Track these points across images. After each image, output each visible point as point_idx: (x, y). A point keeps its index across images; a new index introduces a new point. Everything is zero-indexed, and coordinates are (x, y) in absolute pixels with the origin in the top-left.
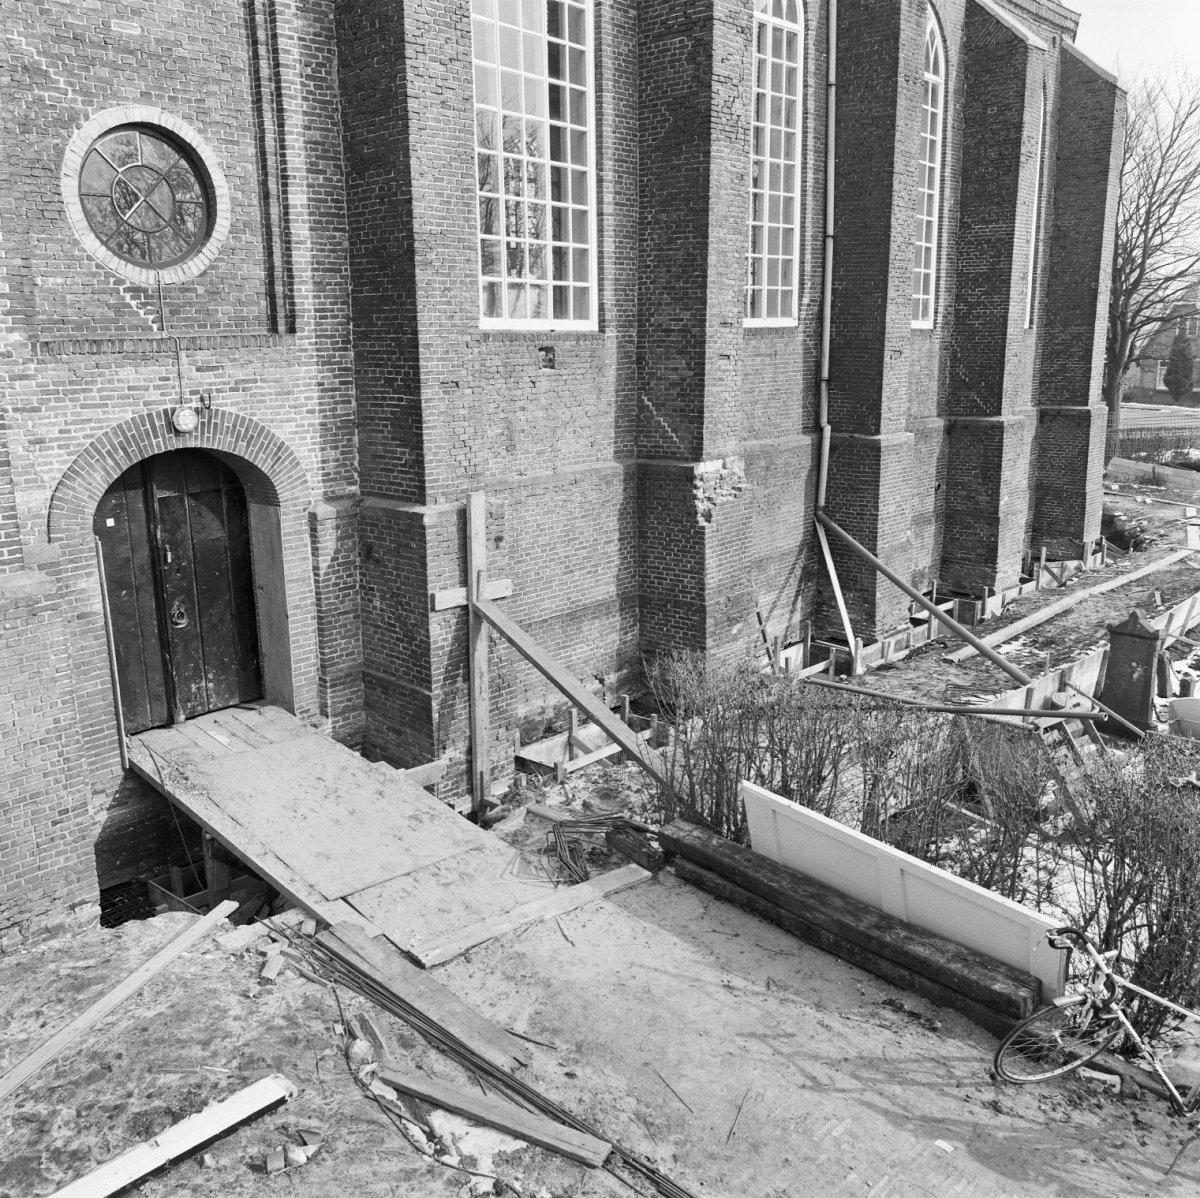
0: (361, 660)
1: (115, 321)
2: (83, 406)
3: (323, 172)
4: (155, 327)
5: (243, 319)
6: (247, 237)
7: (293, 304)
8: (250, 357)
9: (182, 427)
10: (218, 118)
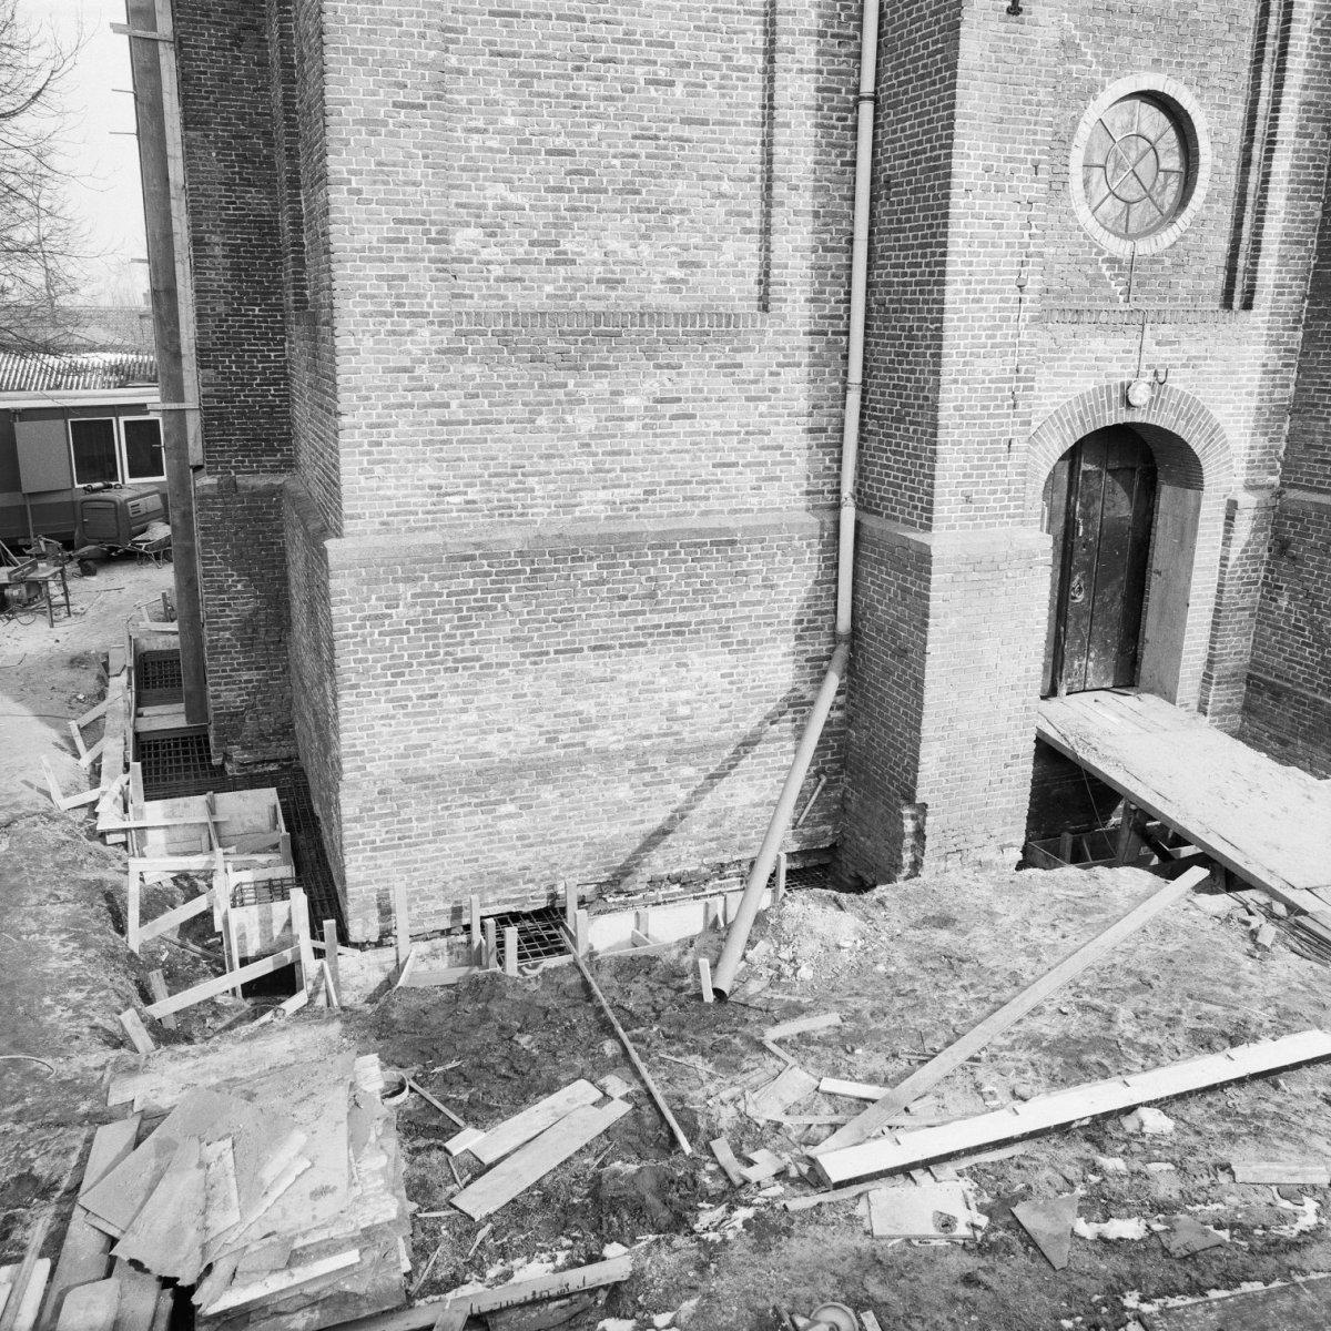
0: (1248, 660)
1: (1088, 291)
2: (1056, 374)
3: (1310, 136)
4: (1122, 298)
5: (1200, 293)
6: (1219, 207)
7: (1254, 279)
8: (1206, 334)
9: (1133, 401)
10: (1217, 82)
